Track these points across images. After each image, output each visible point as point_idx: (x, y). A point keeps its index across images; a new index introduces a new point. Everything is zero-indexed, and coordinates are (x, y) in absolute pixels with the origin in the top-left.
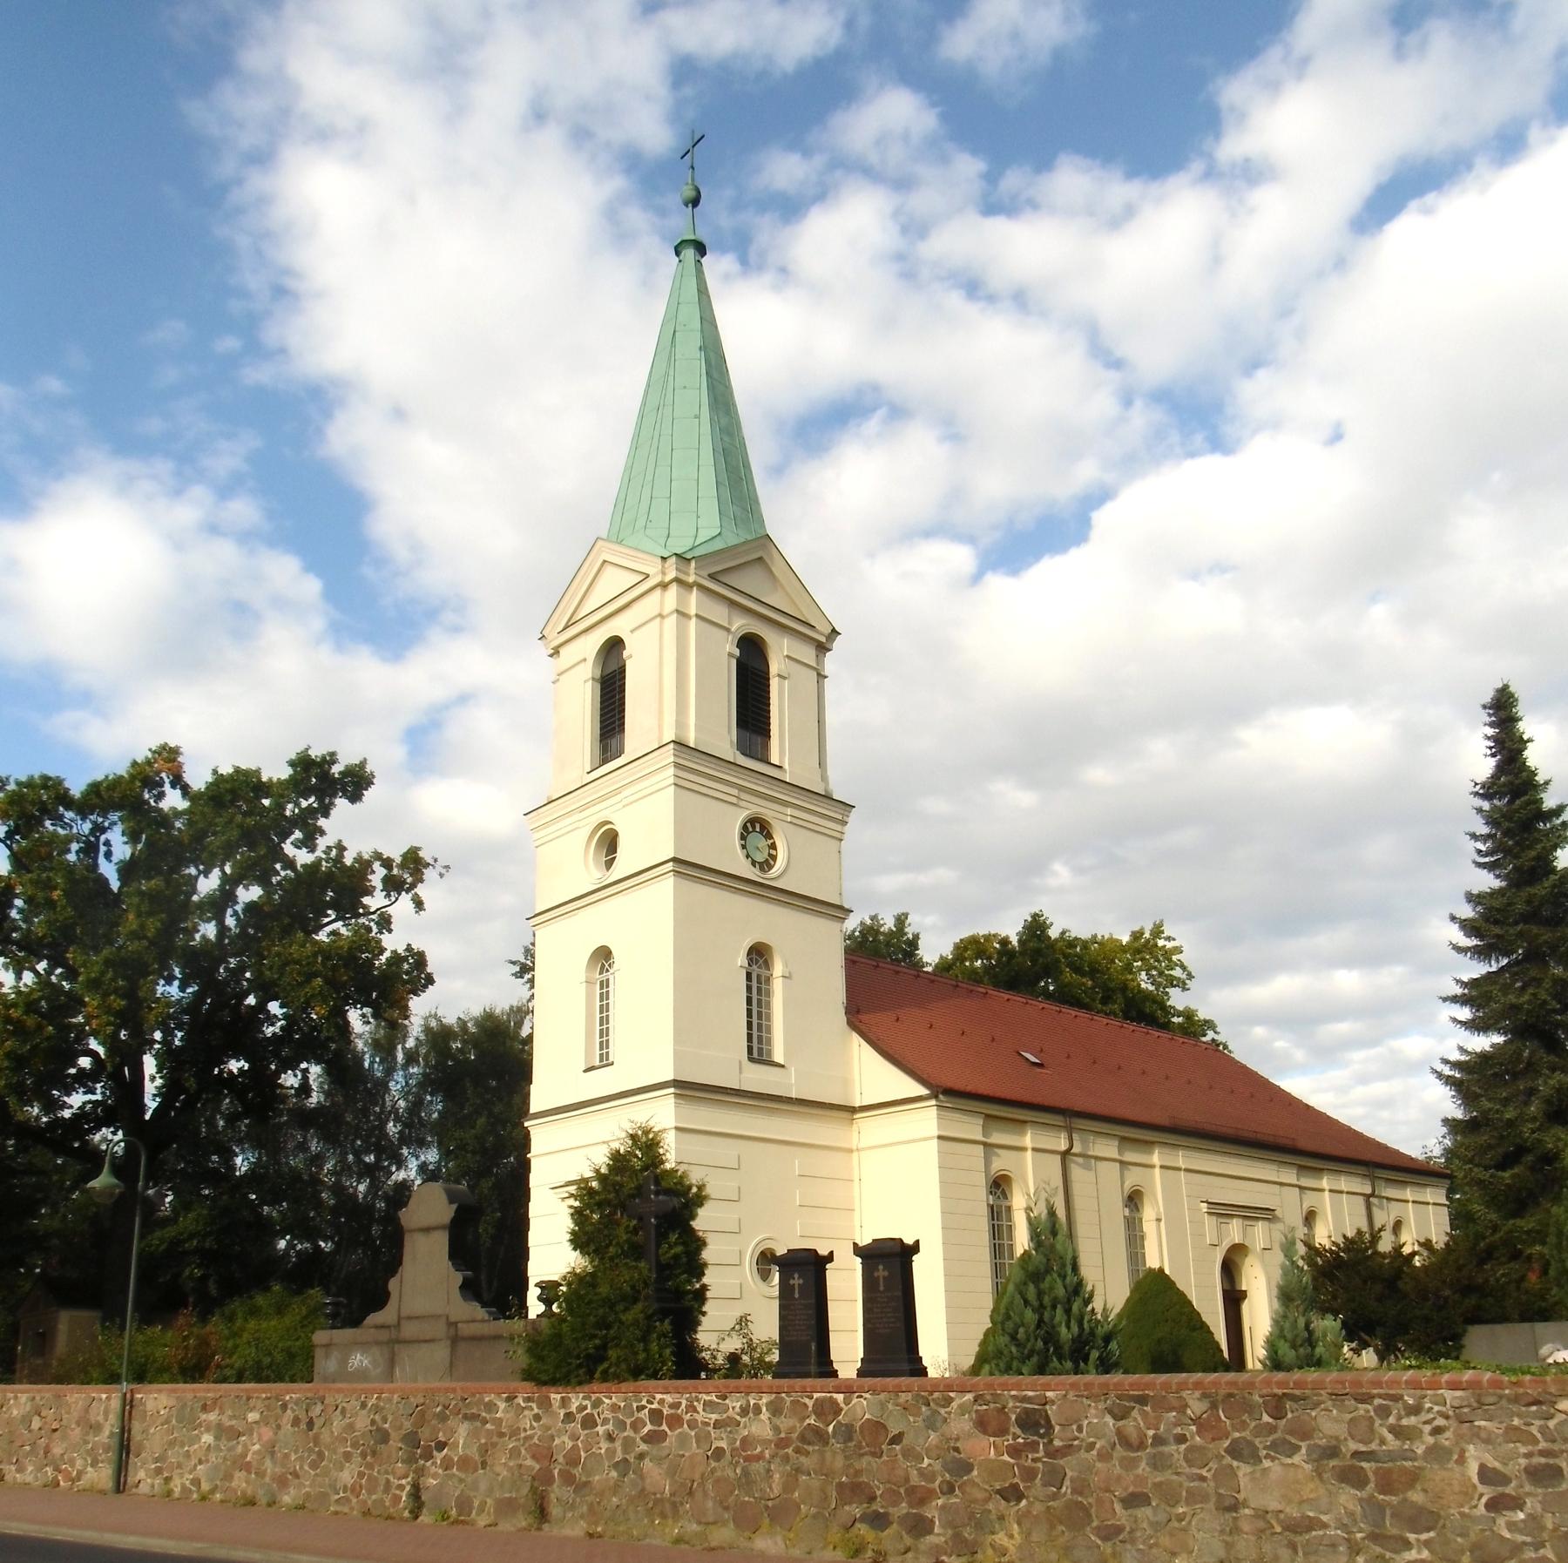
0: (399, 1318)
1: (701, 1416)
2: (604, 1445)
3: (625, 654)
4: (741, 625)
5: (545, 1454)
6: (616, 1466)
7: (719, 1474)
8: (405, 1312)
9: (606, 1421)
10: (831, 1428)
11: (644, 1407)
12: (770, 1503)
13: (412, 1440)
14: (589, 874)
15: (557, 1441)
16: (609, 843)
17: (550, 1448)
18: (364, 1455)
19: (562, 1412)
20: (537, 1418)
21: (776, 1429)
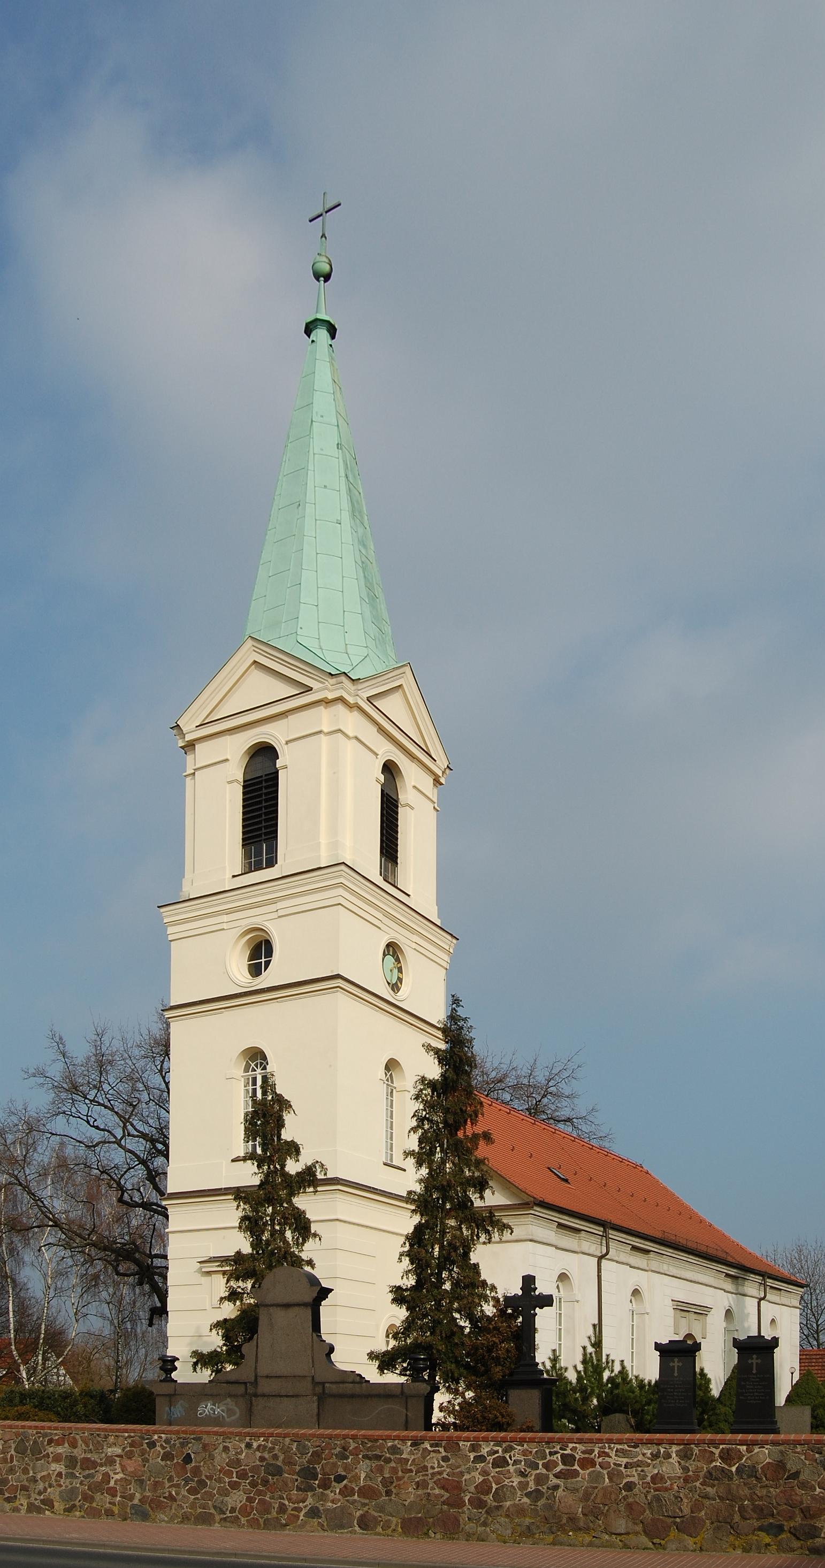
0: (256, 1376)
1: (613, 1459)
2: (516, 1480)
3: (279, 763)
4: (387, 751)
5: (453, 1487)
6: (528, 1495)
7: (631, 1500)
8: (264, 1370)
9: (516, 1463)
10: (734, 1469)
11: (556, 1453)
12: (678, 1520)
13: (308, 1473)
14: (240, 977)
15: (467, 1476)
16: (261, 951)
17: (459, 1482)
18: (253, 1484)
19: (472, 1455)
20: (445, 1459)
21: (685, 1469)
